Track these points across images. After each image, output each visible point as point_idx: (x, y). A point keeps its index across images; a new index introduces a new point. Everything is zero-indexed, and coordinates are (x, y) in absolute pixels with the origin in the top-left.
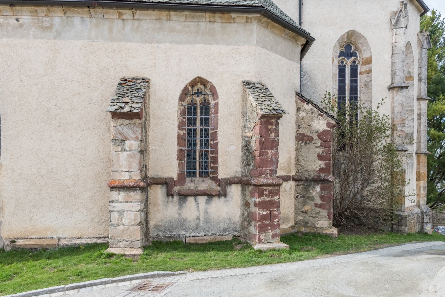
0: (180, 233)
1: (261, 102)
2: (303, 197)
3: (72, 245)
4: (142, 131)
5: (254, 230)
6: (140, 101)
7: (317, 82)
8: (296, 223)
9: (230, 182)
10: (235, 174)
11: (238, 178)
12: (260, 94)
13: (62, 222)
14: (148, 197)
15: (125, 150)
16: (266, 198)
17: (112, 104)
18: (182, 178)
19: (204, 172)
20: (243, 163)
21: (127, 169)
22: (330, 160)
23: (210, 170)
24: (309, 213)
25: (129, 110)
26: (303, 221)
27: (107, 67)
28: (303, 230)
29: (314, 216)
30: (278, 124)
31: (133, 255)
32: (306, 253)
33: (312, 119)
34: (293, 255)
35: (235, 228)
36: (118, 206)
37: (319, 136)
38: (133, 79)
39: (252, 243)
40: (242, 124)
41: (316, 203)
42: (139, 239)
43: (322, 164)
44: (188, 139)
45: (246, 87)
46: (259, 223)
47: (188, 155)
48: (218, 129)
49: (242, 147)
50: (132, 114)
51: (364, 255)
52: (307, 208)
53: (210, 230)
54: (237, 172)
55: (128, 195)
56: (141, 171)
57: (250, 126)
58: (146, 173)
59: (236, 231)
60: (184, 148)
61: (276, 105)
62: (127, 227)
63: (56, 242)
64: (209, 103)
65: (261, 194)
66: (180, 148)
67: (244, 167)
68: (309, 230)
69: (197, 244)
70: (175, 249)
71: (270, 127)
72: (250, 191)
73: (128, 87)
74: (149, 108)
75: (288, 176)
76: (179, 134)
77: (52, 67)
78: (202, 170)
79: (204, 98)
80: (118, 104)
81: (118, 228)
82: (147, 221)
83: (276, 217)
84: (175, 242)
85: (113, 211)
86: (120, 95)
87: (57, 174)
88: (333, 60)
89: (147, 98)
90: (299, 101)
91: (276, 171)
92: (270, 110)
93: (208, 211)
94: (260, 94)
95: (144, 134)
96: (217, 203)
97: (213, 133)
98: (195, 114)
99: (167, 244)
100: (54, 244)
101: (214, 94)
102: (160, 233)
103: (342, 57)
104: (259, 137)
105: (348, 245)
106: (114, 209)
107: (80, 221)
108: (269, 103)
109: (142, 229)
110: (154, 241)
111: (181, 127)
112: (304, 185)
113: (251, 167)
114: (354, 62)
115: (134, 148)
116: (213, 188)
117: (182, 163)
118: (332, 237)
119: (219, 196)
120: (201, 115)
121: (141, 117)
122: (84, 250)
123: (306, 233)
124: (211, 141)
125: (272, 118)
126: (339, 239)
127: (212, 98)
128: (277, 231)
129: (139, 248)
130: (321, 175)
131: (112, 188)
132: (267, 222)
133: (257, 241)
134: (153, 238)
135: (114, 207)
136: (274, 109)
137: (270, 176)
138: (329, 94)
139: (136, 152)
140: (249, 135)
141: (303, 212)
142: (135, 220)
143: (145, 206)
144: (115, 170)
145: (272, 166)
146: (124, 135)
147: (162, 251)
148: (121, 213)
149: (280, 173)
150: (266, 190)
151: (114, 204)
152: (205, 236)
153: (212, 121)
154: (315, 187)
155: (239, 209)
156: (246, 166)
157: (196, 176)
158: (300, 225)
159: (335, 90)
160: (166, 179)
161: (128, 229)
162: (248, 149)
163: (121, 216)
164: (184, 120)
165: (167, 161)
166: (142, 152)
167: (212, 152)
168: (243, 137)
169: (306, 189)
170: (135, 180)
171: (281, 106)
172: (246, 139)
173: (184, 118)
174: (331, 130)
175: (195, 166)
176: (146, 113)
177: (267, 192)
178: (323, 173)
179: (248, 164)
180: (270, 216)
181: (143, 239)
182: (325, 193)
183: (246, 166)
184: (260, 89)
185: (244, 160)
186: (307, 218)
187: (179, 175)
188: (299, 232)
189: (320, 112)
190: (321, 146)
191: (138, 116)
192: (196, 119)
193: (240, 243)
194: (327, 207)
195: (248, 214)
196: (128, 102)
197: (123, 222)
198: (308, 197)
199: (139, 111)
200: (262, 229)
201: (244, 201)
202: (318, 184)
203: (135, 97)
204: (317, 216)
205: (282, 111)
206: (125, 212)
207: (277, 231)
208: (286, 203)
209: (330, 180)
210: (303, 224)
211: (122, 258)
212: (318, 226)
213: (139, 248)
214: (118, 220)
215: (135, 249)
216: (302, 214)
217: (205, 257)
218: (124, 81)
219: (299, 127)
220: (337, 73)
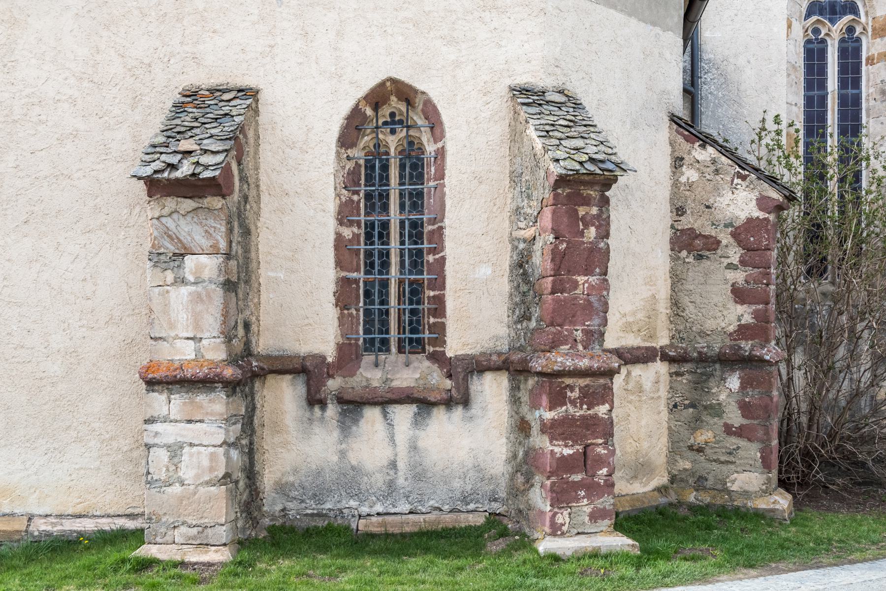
0: (344, 504)
1: (557, 142)
2: (692, 407)
3: (63, 534)
4: (230, 231)
5: (539, 498)
6: (221, 148)
7: (742, 88)
8: (673, 479)
9: (477, 366)
10: (491, 345)
11: (500, 354)
12: (555, 118)
13: (36, 474)
14: (254, 408)
15: (183, 281)
16: (571, 409)
17: (147, 158)
18: (348, 358)
19: (411, 340)
20: (514, 311)
21: (193, 335)
22: (767, 303)
23: (427, 335)
24: (708, 451)
25: (190, 172)
26: (693, 474)
27: (146, 61)
28: (692, 497)
29: (723, 458)
30: (605, 202)
31: (204, 564)
32: (686, 566)
33: (717, 190)
34: (648, 571)
35: (494, 492)
36: (168, 433)
37: (734, 235)
38: (212, 91)
39: (536, 536)
40: (510, 206)
41: (729, 422)
42: (223, 520)
43: (745, 314)
44: (366, 251)
45: (519, 100)
46: (554, 479)
47: (367, 294)
48: (446, 220)
49: (512, 268)
50: (200, 183)
51: (857, 573)
52: (703, 436)
53: (426, 498)
54: (497, 338)
55: (192, 402)
56: (229, 339)
57: (529, 211)
58: (247, 344)
59: (495, 500)
60: (355, 275)
61: (602, 148)
62: (192, 487)
63: (19, 525)
64: (421, 150)
65: (558, 399)
66: (344, 274)
67: (516, 323)
68: (708, 499)
69: (387, 536)
70: (324, 549)
71: (582, 211)
72: (531, 391)
73: (197, 112)
74: (257, 168)
75: (647, 348)
76: (339, 238)
77: (5, 66)
78: (404, 333)
79: (408, 136)
80: (164, 157)
81: (169, 490)
82: (251, 473)
83: (601, 462)
84: (329, 529)
85: (154, 445)
86: (172, 133)
87: (22, 347)
88: (789, 26)
89: (251, 141)
90: (680, 139)
91: (602, 334)
92: (581, 163)
93: (421, 444)
94: (555, 118)
95: (236, 237)
96: (443, 423)
97: (432, 233)
98: (385, 179)
99: (308, 533)
100: (17, 531)
101: (436, 126)
102: (290, 505)
103: (814, 18)
104: (551, 238)
105: (818, 541)
106: (157, 441)
107: (82, 472)
108: (579, 143)
109: (232, 495)
110: (273, 526)
111: (344, 216)
112: (696, 372)
113: (533, 324)
114: (851, 30)
115: (206, 275)
116: (434, 382)
117: (351, 315)
118: (772, 519)
119: (449, 403)
120: (400, 184)
121: (224, 190)
122: (88, 548)
123: (701, 507)
124: (428, 254)
125: (590, 184)
126: (793, 523)
127: (429, 135)
128: (606, 502)
129: (225, 545)
130: (743, 344)
131: (152, 384)
132: (577, 477)
133: (547, 529)
134: (274, 518)
135: (157, 433)
136: (591, 160)
137: (585, 349)
138: (777, 120)
139: (213, 286)
140: (528, 233)
141: (691, 448)
142: (211, 469)
143: (243, 430)
144: (157, 335)
145: (590, 320)
146: (180, 241)
147: (287, 555)
148: (175, 450)
149: (611, 342)
150: (572, 389)
151: (157, 427)
152: (411, 513)
153: (430, 198)
154: (724, 380)
155: (504, 440)
156: (519, 321)
157: (388, 350)
158: (683, 484)
159: (794, 109)
160: (304, 358)
161: (195, 493)
162: (525, 274)
163: (176, 460)
164: (355, 198)
165: (304, 310)
166: (229, 286)
167: (433, 285)
168: (513, 240)
169: (700, 383)
170: (212, 362)
171: (614, 151)
172: (522, 246)
173: (357, 193)
174: (772, 217)
175: (385, 323)
176: (243, 179)
177: (576, 394)
178: (747, 340)
179: (526, 317)
180: (585, 461)
181: (237, 519)
182: (753, 396)
183: (519, 321)
184: (559, 105)
185: (517, 304)
186: (704, 465)
187: (340, 348)
188: (680, 504)
189: (738, 169)
190: (743, 262)
191: (215, 187)
192: (388, 195)
193: (504, 533)
194: (760, 433)
195: (526, 454)
196: (190, 152)
197: (181, 474)
198: (705, 408)
199: (217, 173)
200: (562, 496)
201: (516, 417)
202: (733, 370)
203: (211, 136)
204: (732, 459)
205: (617, 165)
206: (187, 449)
207: (606, 502)
208: (643, 423)
209: (767, 358)
210: (691, 481)
211: (173, 571)
212: (734, 488)
213: (225, 545)
214: (168, 470)
215: (213, 548)
216: (690, 454)
217: (395, 574)
218: (192, 95)
219: (680, 211)
220: (801, 63)
